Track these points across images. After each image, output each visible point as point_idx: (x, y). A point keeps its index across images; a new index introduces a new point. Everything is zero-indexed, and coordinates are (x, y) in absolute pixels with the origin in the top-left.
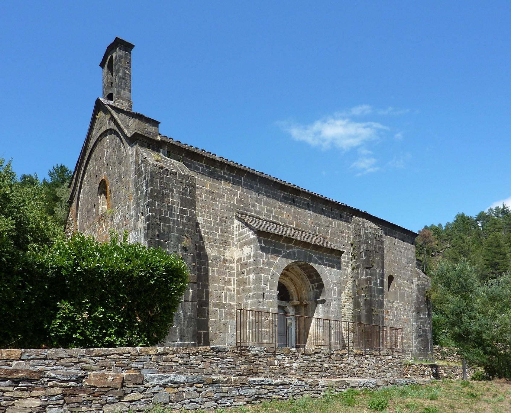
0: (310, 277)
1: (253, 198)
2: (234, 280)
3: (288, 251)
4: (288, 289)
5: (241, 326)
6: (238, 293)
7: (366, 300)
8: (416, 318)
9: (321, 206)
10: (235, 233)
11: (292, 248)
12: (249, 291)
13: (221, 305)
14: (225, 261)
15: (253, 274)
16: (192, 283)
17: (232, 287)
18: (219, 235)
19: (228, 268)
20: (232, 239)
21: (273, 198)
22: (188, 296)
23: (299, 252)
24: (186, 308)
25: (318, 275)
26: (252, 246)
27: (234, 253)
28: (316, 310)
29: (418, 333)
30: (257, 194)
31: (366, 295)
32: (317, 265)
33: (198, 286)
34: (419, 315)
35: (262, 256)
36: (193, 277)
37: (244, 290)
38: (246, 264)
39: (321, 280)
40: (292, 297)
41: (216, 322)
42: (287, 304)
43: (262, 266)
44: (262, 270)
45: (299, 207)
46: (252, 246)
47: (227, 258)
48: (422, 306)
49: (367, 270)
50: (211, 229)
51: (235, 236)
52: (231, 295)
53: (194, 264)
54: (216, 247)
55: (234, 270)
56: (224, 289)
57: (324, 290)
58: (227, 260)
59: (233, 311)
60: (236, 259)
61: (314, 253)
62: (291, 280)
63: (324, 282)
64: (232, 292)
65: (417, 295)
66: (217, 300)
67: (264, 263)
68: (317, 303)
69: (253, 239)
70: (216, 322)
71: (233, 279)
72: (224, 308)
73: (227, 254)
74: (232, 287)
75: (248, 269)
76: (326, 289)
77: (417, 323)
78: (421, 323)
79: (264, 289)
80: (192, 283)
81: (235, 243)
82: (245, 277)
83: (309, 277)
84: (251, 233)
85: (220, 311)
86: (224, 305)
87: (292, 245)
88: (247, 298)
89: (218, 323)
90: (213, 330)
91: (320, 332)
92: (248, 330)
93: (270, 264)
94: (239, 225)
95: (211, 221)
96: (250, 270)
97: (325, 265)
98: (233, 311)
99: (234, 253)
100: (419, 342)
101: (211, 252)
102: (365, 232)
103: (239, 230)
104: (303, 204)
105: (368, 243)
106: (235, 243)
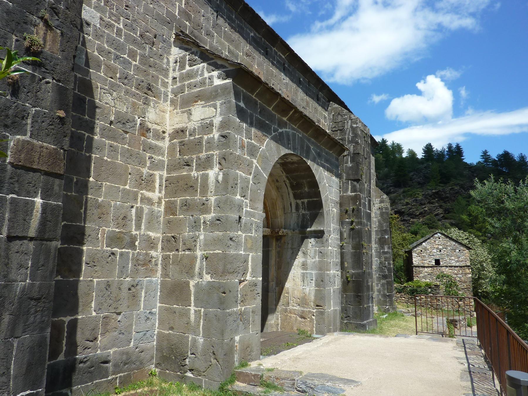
1: (208, 19)
2: (161, 177)
3: (280, 130)
5: (175, 292)
6: (170, 209)
7: (352, 229)
8: (379, 252)
9: (298, 74)
10: (171, 74)
11: (284, 125)
12: (204, 208)
13: (127, 239)
14: (145, 130)
15: (216, 169)
16: (46, 173)
17: (155, 195)
18: (137, 68)
19: (151, 148)
20: (165, 85)
21: (238, 32)
22: (26, 221)
23: (294, 135)
24: (14, 265)
26: (218, 103)
27: (165, 117)
28: (303, 248)
29: (381, 271)
30: (215, 14)
31: (352, 223)
32: (316, 165)
33: (67, 187)
34: (383, 248)
35: (239, 130)
36: (52, 154)
37: (186, 205)
38: (199, 142)
39: (318, 194)
41: (108, 285)
43: (238, 152)
44: (239, 162)
45: (273, 64)
46: (218, 103)
47: (150, 125)
48: (387, 237)
49: (355, 183)
50: (119, 47)
51: (170, 81)
52: (152, 213)
53: (61, 114)
54: (127, 92)
55: (163, 155)
56: (136, 199)
57: (322, 214)
58: (148, 130)
59: (153, 253)
60: (169, 129)
61: (313, 143)
64: (155, 208)
65: (379, 222)
66: (118, 226)
68: (304, 237)
69: (223, 87)
70: (108, 285)
71: (160, 175)
72: (132, 246)
73: (151, 115)
74: (155, 195)
75: (203, 155)
76: (325, 212)
77: (380, 258)
78: (386, 259)
79: (240, 207)
80: (46, 173)
81: (170, 96)
82: (194, 173)
83: (293, 187)
84: (215, 73)
85: (122, 254)
86: (133, 239)
87: (285, 119)
88: (196, 225)
89: (114, 288)
90: (98, 310)
91: (310, 289)
92: (192, 308)
94: (183, 58)
95: (119, 31)
96: (209, 159)
97: (324, 167)
98: (153, 253)
99: (165, 117)
100: (383, 285)
101: (109, 101)
102: (352, 127)
103: (182, 67)
104: (278, 62)
105: (357, 143)
106: (170, 96)
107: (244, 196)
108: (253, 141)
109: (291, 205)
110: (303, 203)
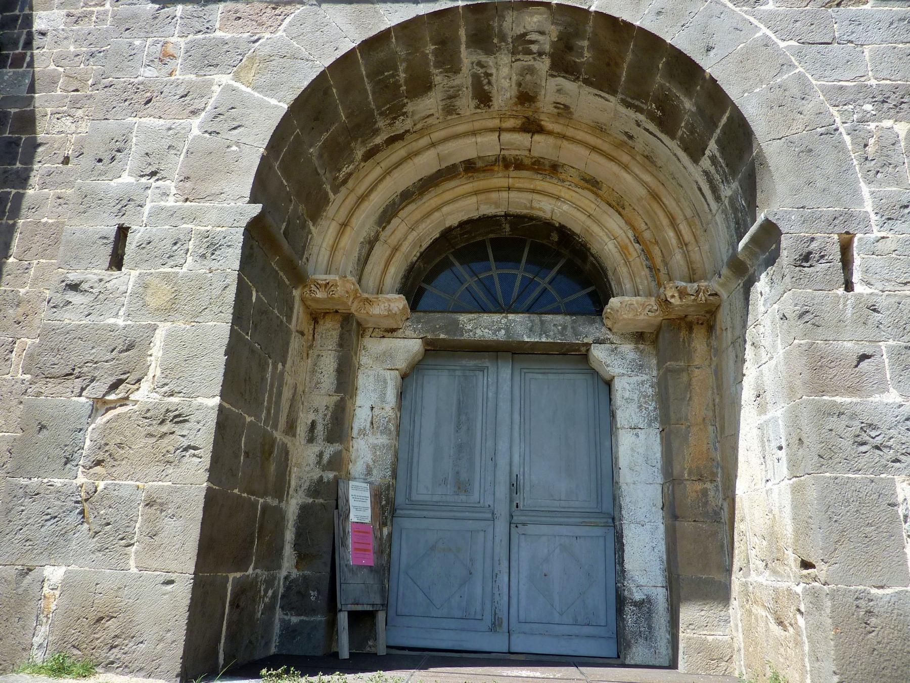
0: (666, 120)
4: (595, 248)
25: (685, 69)
40: (619, 283)
42: (588, 332)
62: (592, 184)
63: (750, 101)
67: (165, 57)
68: (744, 274)
93: (206, 59)
107: (153, 174)
108: (218, 34)
109: (700, 189)
110: (713, 159)
